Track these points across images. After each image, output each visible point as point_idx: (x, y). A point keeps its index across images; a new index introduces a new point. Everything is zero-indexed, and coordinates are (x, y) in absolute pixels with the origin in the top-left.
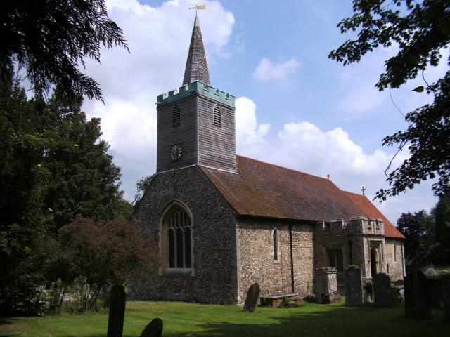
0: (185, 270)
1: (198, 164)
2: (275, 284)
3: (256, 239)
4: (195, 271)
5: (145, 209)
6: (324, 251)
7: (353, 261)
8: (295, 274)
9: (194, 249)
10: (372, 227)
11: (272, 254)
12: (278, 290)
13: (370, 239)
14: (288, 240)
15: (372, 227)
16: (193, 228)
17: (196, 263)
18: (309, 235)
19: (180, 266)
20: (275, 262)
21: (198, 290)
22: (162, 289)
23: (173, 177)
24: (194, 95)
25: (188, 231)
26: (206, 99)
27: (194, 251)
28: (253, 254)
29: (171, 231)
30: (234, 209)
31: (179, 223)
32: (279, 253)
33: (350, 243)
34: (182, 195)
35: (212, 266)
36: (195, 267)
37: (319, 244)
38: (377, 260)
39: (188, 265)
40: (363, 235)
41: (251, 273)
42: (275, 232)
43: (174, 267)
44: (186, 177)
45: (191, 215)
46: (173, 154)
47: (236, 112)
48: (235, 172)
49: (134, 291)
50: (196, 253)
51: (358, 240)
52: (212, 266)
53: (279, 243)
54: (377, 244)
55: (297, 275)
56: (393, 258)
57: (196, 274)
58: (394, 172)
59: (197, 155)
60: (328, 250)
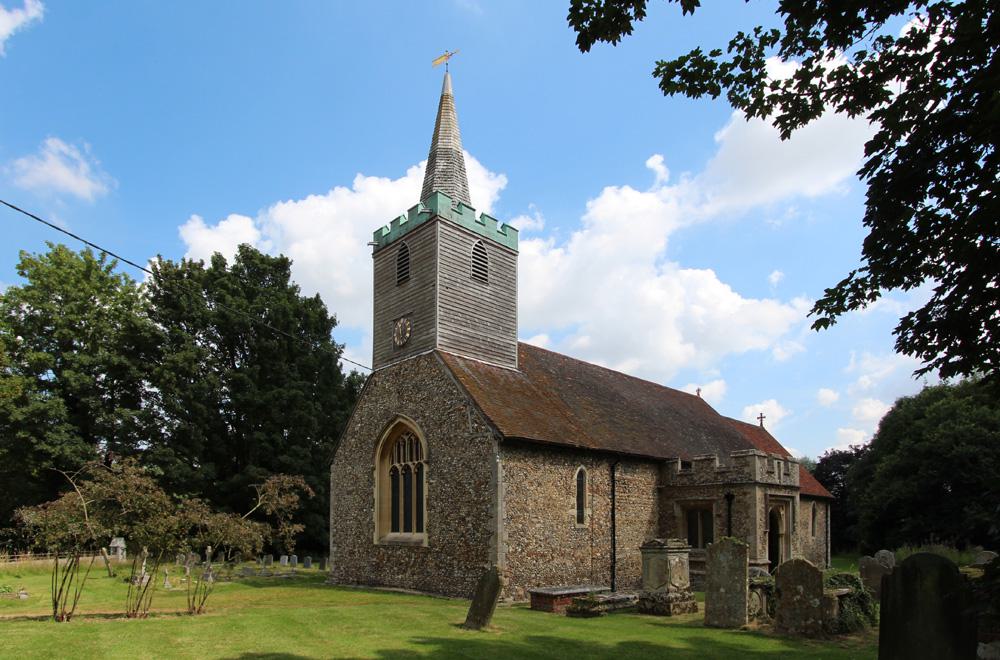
0: (415, 536)
1: (439, 348)
2: (577, 565)
3: (540, 484)
4: (429, 538)
5: (355, 433)
6: (678, 511)
7: (734, 530)
8: (618, 549)
9: (428, 500)
10: (776, 470)
11: (574, 512)
12: (583, 576)
13: (769, 492)
14: (608, 489)
15: (776, 470)
16: (427, 463)
17: (430, 525)
18: (649, 484)
19: (408, 529)
20: (578, 526)
21: (433, 572)
22: (378, 567)
23: (396, 374)
24: (433, 218)
25: (420, 467)
26: (458, 227)
27: (428, 503)
28: (534, 512)
29: (394, 470)
30: (494, 426)
31: (408, 456)
32: (588, 512)
33: (729, 498)
34: (411, 406)
35: (456, 530)
36: (428, 531)
37: (668, 498)
38: (783, 530)
39: (420, 529)
40: (756, 483)
41: (528, 545)
42: (581, 474)
43: (398, 531)
44: (416, 374)
45: (423, 442)
46: (398, 334)
47: (520, 258)
48: (514, 367)
49: (338, 568)
50: (431, 507)
51: (745, 494)
52: (456, 530)
53: (588, 493)
54: (785, 502)
55: (622, 551)
56: (810, 530)
57: (430, 544)
58: (852, 275)
59: (435, 332)
60: (683, 508)
